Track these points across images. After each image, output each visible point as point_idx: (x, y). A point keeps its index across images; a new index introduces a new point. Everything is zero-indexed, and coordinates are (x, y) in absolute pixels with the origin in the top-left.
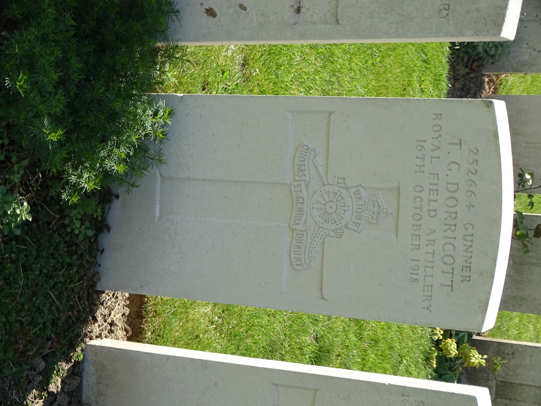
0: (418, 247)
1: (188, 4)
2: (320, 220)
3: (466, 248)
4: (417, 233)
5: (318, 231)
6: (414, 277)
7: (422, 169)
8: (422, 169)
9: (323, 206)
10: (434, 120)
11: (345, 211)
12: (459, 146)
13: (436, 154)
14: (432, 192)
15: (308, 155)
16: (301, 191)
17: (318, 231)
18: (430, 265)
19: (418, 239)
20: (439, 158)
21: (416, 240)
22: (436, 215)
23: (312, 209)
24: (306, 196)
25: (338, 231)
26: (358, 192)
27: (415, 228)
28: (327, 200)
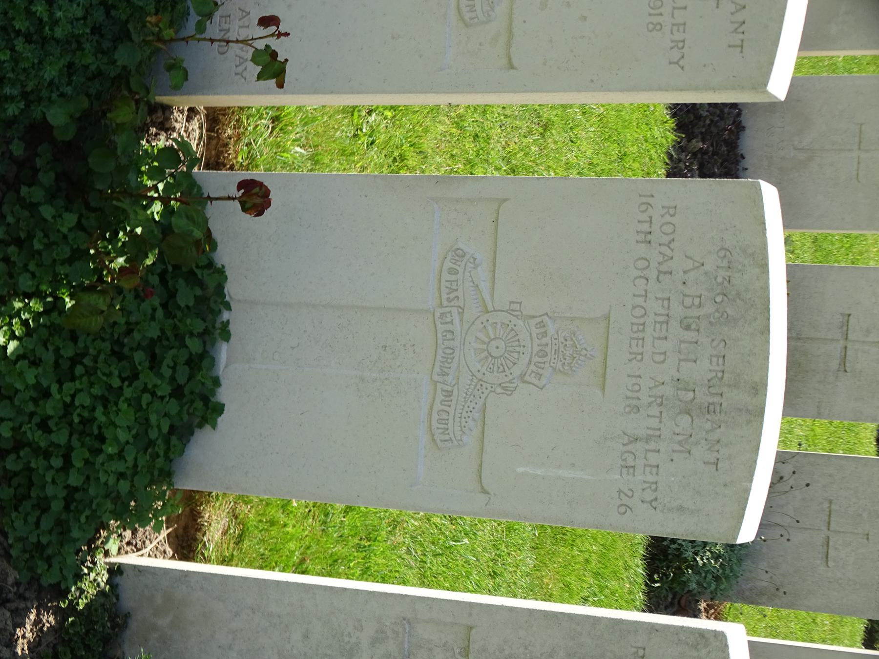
1: (254, 197)
2: (479, 367)
5: (476, 386)
6: (655, 19)
8: (649, 237)
9: (485, 346)
10: (662, 216)
14: (675, 28)
15: (453, 407)
17: (476, 386)
20: (659, 451)
22: (665, 360)
24: (459, 329)
25: (508, 385)
26: (542, 325)
28: (492, 337)
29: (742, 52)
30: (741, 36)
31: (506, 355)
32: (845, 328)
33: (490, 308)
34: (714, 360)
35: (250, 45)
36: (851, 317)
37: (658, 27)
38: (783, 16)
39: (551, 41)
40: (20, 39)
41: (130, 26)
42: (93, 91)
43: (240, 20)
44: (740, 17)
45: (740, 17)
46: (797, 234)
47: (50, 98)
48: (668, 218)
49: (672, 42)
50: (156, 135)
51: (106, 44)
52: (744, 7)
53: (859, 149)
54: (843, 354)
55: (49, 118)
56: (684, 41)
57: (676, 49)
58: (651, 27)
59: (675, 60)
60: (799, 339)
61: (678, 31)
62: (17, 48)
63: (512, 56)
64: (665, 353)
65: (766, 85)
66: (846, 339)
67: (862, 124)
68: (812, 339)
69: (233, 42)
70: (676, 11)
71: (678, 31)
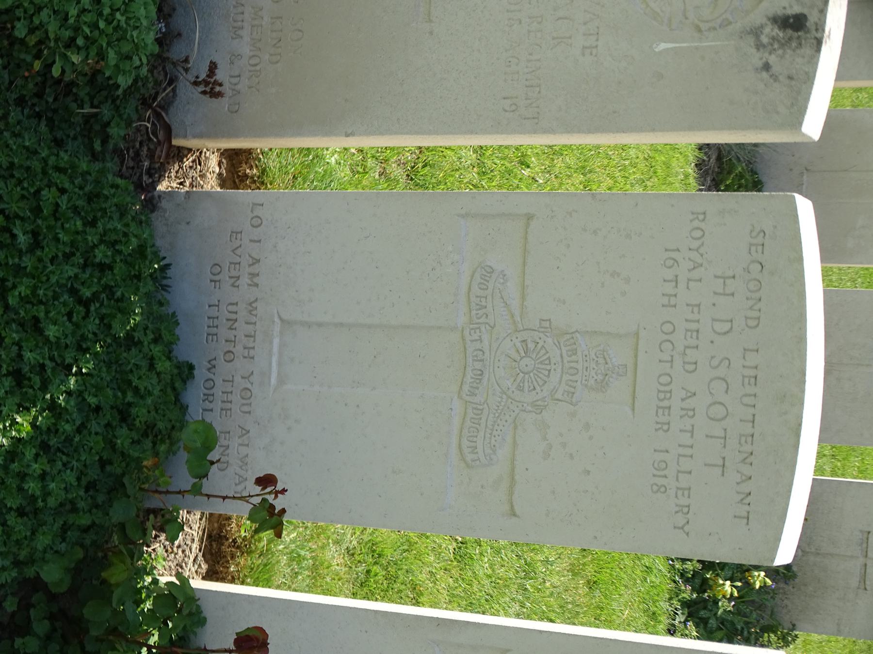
0: (669, 395)
3: (751, 303)
4: (666, 403)
6: (661, 481)
7: (673, 301)
8: (673, 301)
11: (549, 371)
12: (721, 469)
13: (696, 274)
16: (481, 340)
18: (689, 451)
19: (666, 413)
21: (664, 415)
23: (496, 368)
25: (539, 403)
27: (662, 396)
29: (748, 524)
30: (747, 508)
31: (532, 374)
32: (865, 545)
33: (520, 327)
34: (753, 249)
35: (247, 502)
36: (870, 535)
37: (663, 489)
38: (790, 491)
39: (553, 492)
40: (12, 513)
41: (126, 480)
42: (88, 542)
43: (239, 437)
44: (745, 488)
45: (745, 488)
47: (43, 559)
48: (696, 223)
49: (677, 505)
50: (156, 536)
51: (101, 498)
52: (750, 478)
54: (863, 572)
55: (43, 576)
56: (689, 506)
57: (680, 514)
58: (655, 488)
59: (680, 525)
60: (818, 554)
61: (683, 495)
62: (9, 523)
63: (514, 504)
64: (696, 363)
65: (800, 124)
66: (866, 556)
68: (832, 555)
69: (230, 498)
70: (680, 474)
71: (683, 495)
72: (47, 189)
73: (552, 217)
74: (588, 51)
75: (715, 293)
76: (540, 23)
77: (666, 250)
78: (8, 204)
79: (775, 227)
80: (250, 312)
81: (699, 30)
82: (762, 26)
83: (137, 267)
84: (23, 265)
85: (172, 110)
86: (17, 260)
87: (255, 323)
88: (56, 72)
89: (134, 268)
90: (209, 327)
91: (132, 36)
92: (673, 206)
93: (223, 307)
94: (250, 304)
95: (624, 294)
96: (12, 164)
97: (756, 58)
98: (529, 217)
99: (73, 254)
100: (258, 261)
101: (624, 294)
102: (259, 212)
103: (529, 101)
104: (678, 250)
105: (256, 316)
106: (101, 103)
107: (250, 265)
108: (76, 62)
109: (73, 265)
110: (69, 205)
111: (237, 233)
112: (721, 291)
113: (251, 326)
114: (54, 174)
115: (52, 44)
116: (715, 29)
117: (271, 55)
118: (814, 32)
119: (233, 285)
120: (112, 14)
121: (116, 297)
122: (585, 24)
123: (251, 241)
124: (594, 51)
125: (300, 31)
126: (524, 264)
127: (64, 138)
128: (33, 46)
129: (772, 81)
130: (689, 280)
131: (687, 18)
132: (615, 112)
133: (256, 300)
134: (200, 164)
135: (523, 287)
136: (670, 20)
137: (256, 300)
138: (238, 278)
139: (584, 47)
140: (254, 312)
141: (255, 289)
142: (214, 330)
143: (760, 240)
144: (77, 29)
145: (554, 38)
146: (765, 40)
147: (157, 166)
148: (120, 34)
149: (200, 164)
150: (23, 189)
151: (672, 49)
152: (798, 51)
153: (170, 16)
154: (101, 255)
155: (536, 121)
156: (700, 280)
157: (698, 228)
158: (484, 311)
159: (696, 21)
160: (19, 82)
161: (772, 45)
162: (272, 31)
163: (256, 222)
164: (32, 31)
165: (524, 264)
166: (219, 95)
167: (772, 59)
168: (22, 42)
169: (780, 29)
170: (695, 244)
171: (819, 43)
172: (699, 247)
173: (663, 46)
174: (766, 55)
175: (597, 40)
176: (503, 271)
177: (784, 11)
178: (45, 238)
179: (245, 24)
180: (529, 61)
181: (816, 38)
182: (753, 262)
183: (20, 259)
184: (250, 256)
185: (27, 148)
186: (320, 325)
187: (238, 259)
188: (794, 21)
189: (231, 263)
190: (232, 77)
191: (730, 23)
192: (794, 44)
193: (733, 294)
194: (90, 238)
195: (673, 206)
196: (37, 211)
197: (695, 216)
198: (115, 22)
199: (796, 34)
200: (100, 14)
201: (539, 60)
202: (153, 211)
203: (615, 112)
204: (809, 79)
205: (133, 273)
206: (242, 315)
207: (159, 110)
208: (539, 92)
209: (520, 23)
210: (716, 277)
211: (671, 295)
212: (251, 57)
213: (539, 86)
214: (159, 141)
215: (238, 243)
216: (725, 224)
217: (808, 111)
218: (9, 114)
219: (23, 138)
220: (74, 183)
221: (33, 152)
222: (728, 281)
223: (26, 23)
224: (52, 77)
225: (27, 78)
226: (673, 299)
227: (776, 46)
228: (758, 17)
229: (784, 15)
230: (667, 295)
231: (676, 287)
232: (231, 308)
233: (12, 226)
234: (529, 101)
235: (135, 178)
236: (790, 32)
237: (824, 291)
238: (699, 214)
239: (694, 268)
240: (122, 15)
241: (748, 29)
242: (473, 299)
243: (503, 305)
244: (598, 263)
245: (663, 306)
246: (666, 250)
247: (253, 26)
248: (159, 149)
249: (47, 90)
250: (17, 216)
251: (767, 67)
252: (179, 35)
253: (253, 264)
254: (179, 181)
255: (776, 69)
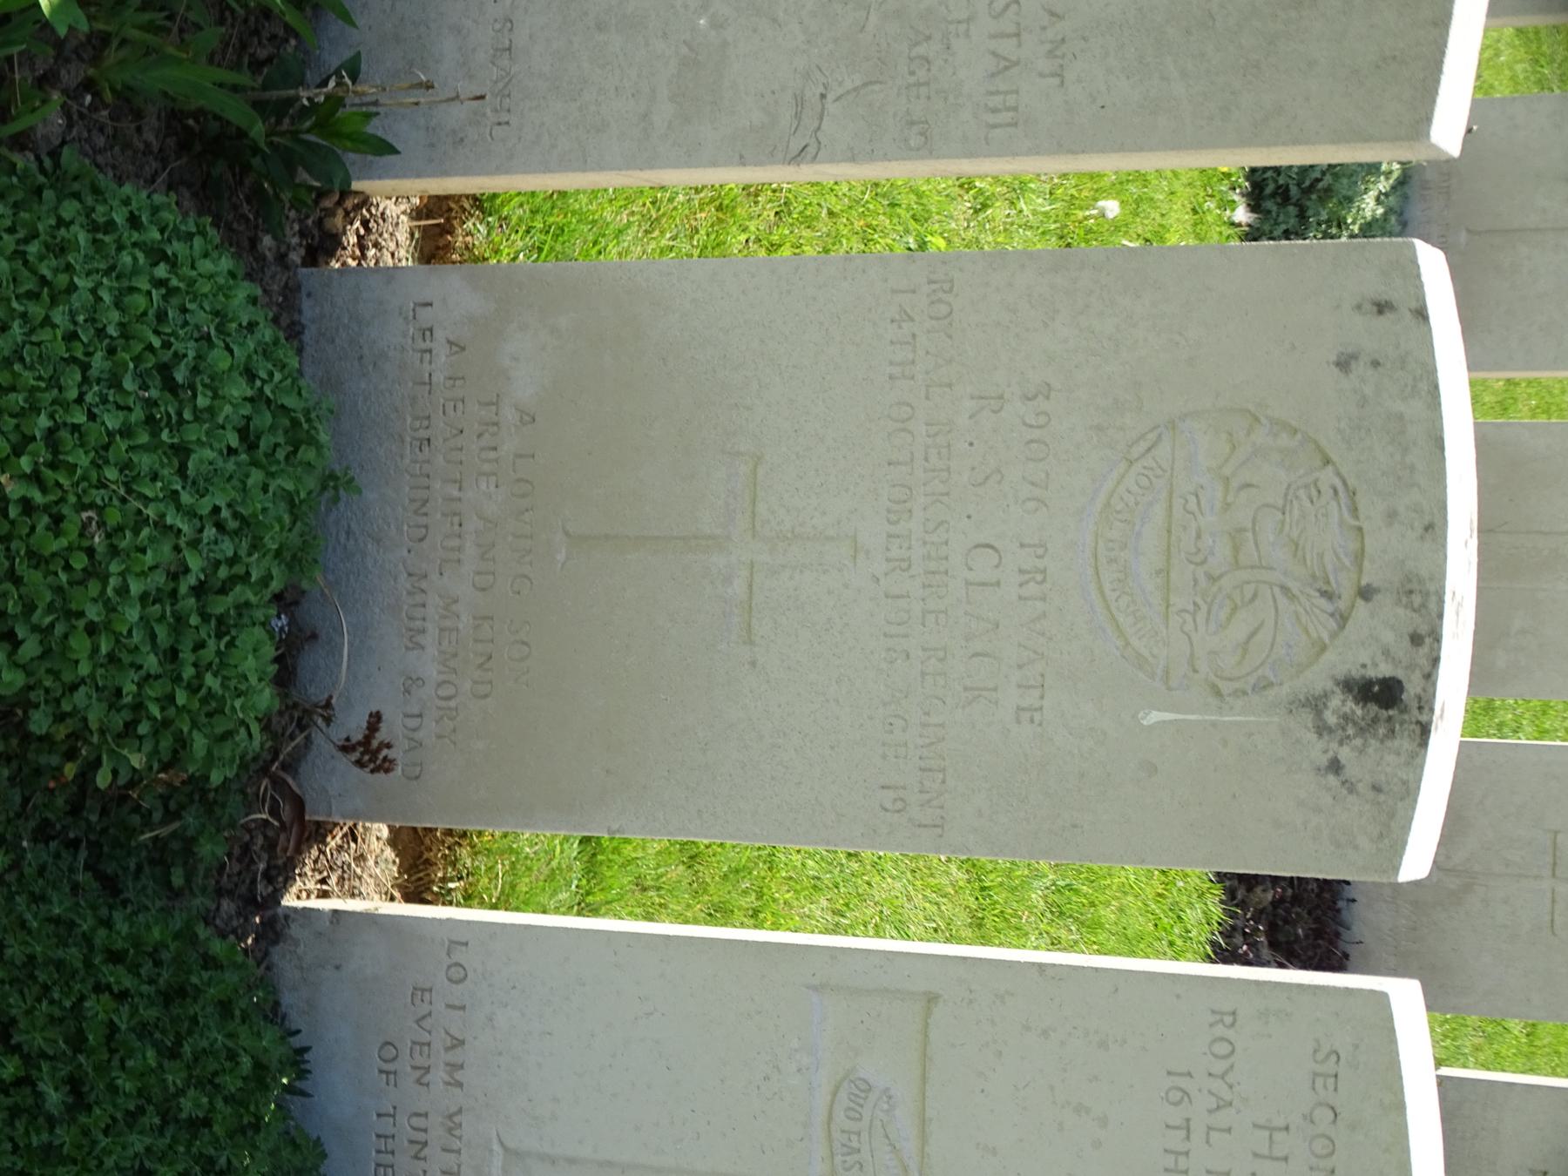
13: (1223, 1118)
34: (1319, 1082)
46: (1497, 378)
48: (1220, 1030)
53: (1554, 875)
64: (1234, 1013)
67: (1556, 833)
72: (93, 996)
73: (971, 1001)
74: (1026, 716)
75: (1256, 1155)
76: (941, 660)
77: (1169, 1073)
78: (28, 1032)
79: (1356, 1047)
80: (450, 1131)
81: (1218, 693)
82: (1326, 695)
83: (252, 1108)
84: (57, 1142)
85: (304, 768)
86: (45, 1137)
87: (459, 1152)
88: (103, 779)
89: (247, 1108)
90: (379, 1152)
91: (233, 708)
92: (1178, 996)
93: (402, 1119)
94: (450, 1117)
95: (1097, 1144)
96: (31, 958)
97: (1318, 750)
98: (932, 999)
99: (141, 1111)
100: (462, 1042)
101: (1097, 1144)
102: (459, 956)
103: (927, 796)
104: (1189, 1074)
105: (460, 1138)
106: (182, 807)
107: (447, 1049)
108: (137, 766)
109: (141, 1133)
110: (133, 1022)
111: (423, 990)
112: (1266, 1152)
113: (453, 1156)
114: (104, 969)
115: (95, 739)
116: (1245, 693)
117: (475, 682)
118: (1415, 712)
119: (419, 1082)
120: (199, 676)
121: (217, 1168)
122: (1020, 667)
123: (448, 1006)
124: (1037, 716)
125: (524, 643)
126: (924, 1078)
127: (120, 872)
128: (63, 742)
129: (1345, 792)
130: (1210, 1128)
131: (1195, 671)
132: (1075, 826)
133: (460, 1111)
134: (355, 841)
135: (923, 1122)
136: (1167, 672)
137: (460, 1111)
138: (427, 1070)
139: (1020, 709)
140: (457, 1132)
141: (457, 1091)
142: (388, 1159)
143: (1330, 1067)
144: (138, 707)
145: (966, 689)
146: (1331, 719)
147: (280, 862)
148: (214, 707)
149: (355, 841)
150: (52, 1002)
151: (1171, 722)
152: (1389, 743)
153: (296, 603)
154: (189, 1104)
155: (939, 831)
156: (1229, 1130)
157: (1222, 1039)
158: (856, 1157)
159: (1212, 677)
160: (38, 798)
161: (1344, 729)
162: (476, 641)
163: (456, 973)
164: (60, 718)
165: (924, 1078)
166: (386, 766)
167: (1345, 754)
168: (46, 739)
169: (1357, 701)
170: (1218, 1067)
171: (1425, 731)
172: (1226, 1073)
173: (1155, 717)
174: (1334, 745)
175: (1042, 697)
176: (888, 1089)
177: (1363, 671)
178: (92, 1089)
179: (429, 625)
180: (924, 725)
181: (1418, 722)
182: (1320, 1104)
183: (51, 1131)
184: (447, 1033)
185: (56, 921)
186: (572, 1161)
187: (426, 1037)
188: (1381, 690)
189: (414, 1043)
190: (407, 716)
191: (1271, 684)
192: (1382, 731)
193: (1286, 1159)
194: (170, 1078)
195: (1178, 996)
196: (78, 1042)
197: (1218, 1017)
198: (204, 691)
199: (1384, 714)
200: (178, 679)
201: (942, 725)
202: (275, 942)
203: (1075, 826)
204: (1409, 792)
205: (245, 1121)
206: (436, 1134)
207: (282, 774)
208: (944, 782)
209: (908, 656)
210: (1255, 1126)
211: (1178, 1153)
212: (439, 685)
213: (943, 770)
214: (283, 825)
215: (425, 1009)
216: (1270, 1036)
217: (1408, 848)
218: (23, 858)
219: (51, 902)
220: (139, 975)
221: (63, 927)
222: (1278, 1136)
223: (49, 710)
224: (97, 789)
225: (52, 791)
226: (1182, 1159)
227: (1350, 731)
228: (1318, 678)
229: (1363, 677)
230: (1172, 1152)
231: (1188, 1138)
232: (415, 1121)
233: (34, 1073)
234: (927, 796)
235: (243, 889)
236: (1373, 708)
237: (1476, 425)
238: (1222, 1014)
239: (1218, 1108)
240: (215, 675)
241: (1302, 697)
242: (836, 1135)
243: (889, 1148)
244: (1052, 1088)
245: (1166, 1170)
246: (1169, 1073)
247: (442, 630)
248: (282, 837)
249: (88, 803)
250: (43, 1055)
251: (1335, 766)
252: (314, 636)
253: (453, 1047)
254: (318, 877)
255: (1352, 770)
